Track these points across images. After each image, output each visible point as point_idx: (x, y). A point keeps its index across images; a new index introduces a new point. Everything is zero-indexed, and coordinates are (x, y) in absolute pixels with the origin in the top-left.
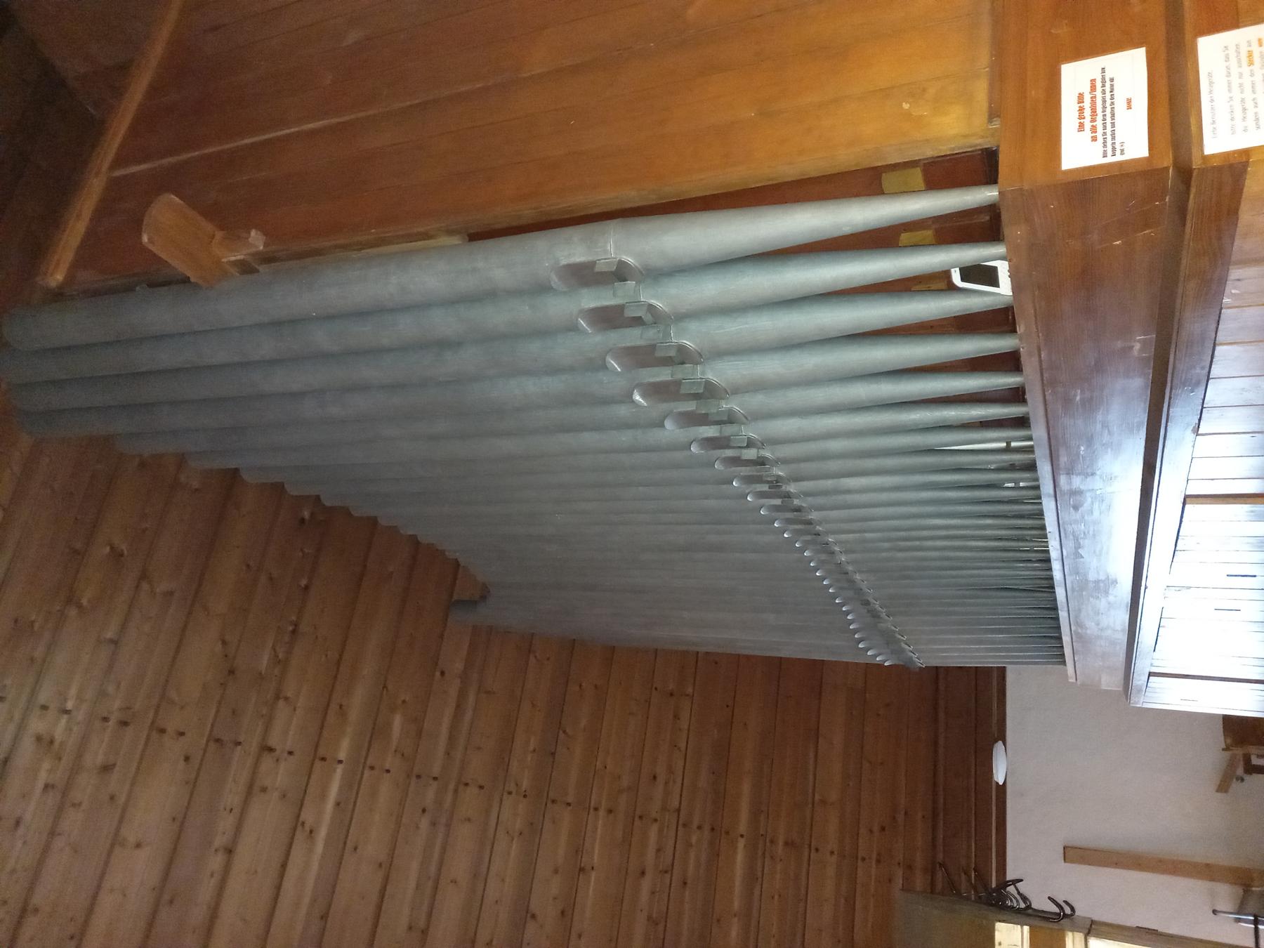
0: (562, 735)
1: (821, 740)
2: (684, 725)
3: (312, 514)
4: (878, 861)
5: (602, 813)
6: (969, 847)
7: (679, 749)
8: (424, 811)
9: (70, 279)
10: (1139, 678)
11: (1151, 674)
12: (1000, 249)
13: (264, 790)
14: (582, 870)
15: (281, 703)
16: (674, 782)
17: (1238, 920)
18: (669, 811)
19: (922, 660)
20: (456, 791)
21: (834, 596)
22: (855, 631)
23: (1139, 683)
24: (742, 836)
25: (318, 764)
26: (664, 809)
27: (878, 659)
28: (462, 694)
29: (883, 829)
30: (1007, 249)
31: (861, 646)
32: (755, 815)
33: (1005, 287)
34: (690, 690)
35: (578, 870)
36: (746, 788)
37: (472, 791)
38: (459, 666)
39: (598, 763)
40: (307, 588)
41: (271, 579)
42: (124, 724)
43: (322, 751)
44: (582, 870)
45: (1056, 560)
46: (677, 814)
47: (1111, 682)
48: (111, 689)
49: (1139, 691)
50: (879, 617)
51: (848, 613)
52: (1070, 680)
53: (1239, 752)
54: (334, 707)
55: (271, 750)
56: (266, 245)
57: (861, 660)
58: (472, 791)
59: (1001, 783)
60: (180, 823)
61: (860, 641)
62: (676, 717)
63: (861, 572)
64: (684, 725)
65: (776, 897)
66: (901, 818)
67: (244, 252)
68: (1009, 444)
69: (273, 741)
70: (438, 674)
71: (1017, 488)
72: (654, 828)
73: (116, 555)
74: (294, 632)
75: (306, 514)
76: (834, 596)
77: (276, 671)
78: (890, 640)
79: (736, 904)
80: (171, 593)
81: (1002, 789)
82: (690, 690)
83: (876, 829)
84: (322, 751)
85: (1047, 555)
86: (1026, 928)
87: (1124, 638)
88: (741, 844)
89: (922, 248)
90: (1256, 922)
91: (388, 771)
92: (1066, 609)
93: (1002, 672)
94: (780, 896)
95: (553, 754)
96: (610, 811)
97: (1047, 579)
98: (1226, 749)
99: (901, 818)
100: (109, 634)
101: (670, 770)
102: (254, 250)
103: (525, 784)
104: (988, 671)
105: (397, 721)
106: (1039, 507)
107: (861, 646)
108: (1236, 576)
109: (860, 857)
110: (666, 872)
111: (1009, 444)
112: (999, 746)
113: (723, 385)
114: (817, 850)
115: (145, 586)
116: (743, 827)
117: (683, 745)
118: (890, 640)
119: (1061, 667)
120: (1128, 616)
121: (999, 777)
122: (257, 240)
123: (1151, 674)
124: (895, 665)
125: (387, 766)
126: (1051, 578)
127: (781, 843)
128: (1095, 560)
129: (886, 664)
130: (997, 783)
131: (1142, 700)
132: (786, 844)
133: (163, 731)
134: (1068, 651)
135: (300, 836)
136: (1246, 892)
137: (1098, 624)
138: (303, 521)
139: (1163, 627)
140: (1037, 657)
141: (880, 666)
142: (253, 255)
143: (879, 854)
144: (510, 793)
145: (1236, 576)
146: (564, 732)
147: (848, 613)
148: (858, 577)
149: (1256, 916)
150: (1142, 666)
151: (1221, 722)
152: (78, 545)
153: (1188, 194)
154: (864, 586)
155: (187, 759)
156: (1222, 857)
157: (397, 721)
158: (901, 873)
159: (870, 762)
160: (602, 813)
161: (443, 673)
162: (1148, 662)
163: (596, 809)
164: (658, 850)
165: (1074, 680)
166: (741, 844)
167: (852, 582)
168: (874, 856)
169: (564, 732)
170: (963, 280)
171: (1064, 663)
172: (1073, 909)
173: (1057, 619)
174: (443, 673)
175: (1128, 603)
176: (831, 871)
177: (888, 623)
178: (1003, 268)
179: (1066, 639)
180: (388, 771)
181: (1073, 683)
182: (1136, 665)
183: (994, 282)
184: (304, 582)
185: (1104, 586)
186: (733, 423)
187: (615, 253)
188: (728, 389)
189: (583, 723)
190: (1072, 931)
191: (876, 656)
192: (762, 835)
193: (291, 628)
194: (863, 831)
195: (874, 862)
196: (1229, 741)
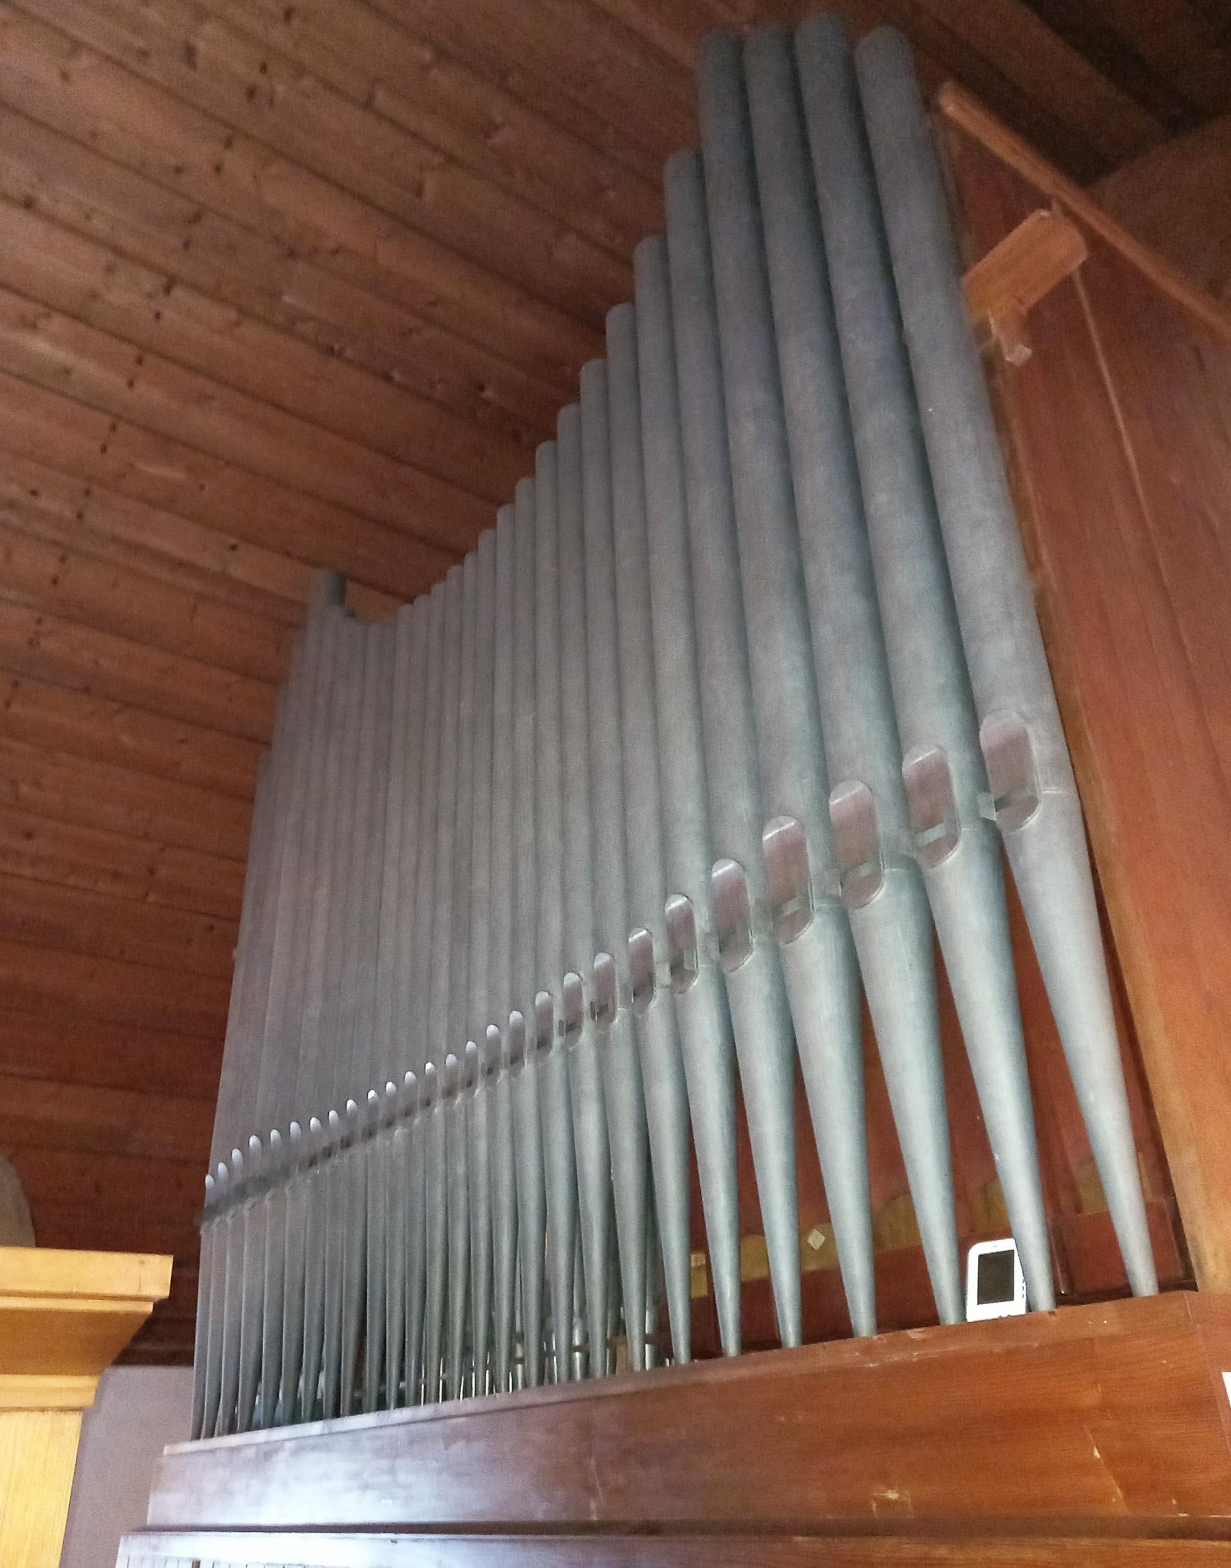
0: (115, 706)
2: (101, 886)
3: (487, 403)
8: (34, 493)
9: (949, 123)
12: (1044, 1301)
13: (110, 269)
15: (233, 316)
20: (55, 543)
21: (360, 1098)
25: (132, 352)
28: (199, 572)
30: (952, 1326)
31: (253, 1140)
33: (978, 1312)
37: (50, 566)
38: (238, 571)
40: (388, 378)
41: (411, 331)
42: (251, 93)
43: (150, 360)
45: (436, 1410)
48: (307, 83)
51: (323, 1119)
54: (209, 387)
55: (168, 290)
56: (1011, 365)
57: (216, 1141)
58: (50, 566)
60: (89, 143)
61: (264, 1139)
62: (116, 876)
63: (409, 1137)
64: (101, 886)
67: (1002, 337)
68: (578, 1349)
69: (178, 293)
70: (233, 541)
71: (572, 1349)
73: (490, 129)
74: (331, 350)
75: (489, 394)
76: (360, 1098)
77: (280, 319)
80: (419, 192)
82: (152, 898)
84: (150, 360)
85: (450, 1398)
89: (736, 1261)
91: (104, 450)
95: (87, 690)
97: (418, 1394)
100: (381, 97)
102: (1005, 349)
103: (48, 644)
105: (176, 474)
106: (433, 1399)
107: (253, 1140)
111: (521, 1361)
113: (801, 937)
115: (437, 160)
117: (71, 881)
119: (190, 1434)
122: (1018, 354)
125: (110, 450)
133: (228, 144)
135: (31, 309)
138: (482, 388)
141: (204, 1166)
142: (998, 346)
144: (39, 621)
146: (118, 711)
147: (323, 1119)
152: (514, 80)
153: (1212, 1539)
155: (179, 170)
157: (176, 474)
161: (234, 548)
169: (118, 711)
170: (983, 1258)
174: (234, 548)
178: (1015, 1307)
180: (104, 450)
183: (985, 1296)
184: (396, 375)
186: (720, 952)
187: (1046, 795)
188: (791, 944)
189: (127, 740)
191: (228, 1161)
193: (336, 347)
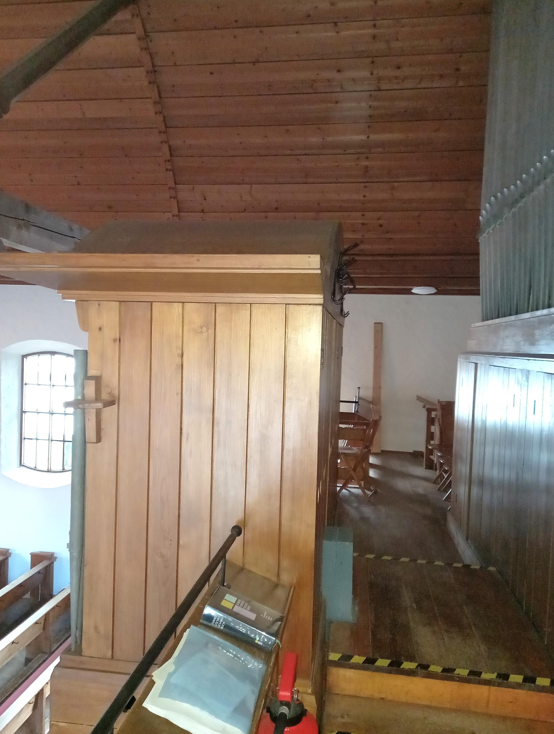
1: (430, 183)
4: (363, 224)
5: (372, 31)
6: (376, 274)
7: (419, 83)
10: (473, 359)
11: (476, 364)
14: (336, 24)
16: (398, 83)
17: (356, 396)
18: (379, 83)
19: (483, 239)
21: (527, 173)
22: (502, 193)
23: (471, 358)
24: (368, 137)
26: (379, 79)
27: (484, 211)
29: (381, 226)
31: (492, 198)
32: (382, 144)
34: (461, 84)
35: (336, 21)
36: (396, 136)
39: (405, 20)
44: (336, 24)
46: (377, 89)
47: (472, 344)
49: (466, 359)
50: (512, 207)
51: (515, 185)
52: (472, 325)
53: (438, 407)
59: (413, 291)
61: (496, 197)
62: (441, 76)
65: (336, 164)
66: (388, 236)
72: (365, 73)
76: (527, 173)
78: (496, 217)
79: (330, 139)
81: (408, 292)
83: (381, 222)
86: (319, 272)
87: (498, 351)
88: (364, 137)
90: (355, 402)
92: (516, 319)
93: (476, 293)
94: (337, 166)
96: (374, 37)
97: (537, 306)
98: (439, 402)
99: (388, 236)
101: (405, 78)
104: (478, 284)
108: (535, 405)
109: (364, 213)
110: (342, 88)
112: (433, 290)
114: (365, 187)
116: (373, 137)
117: (423, 85)
118: (496, 217)
119: (481, 318)
120: (511, 352)
121: (415, 290)
123: (476, 364)
124: (480, 223)
126: (537, 309)
127: (367, 163)
128: (548, 333)
129: (481, 218)
130: (412, 289)
131: (461, 360)
132: (367, 167)
134: (490, 322)
136: (370, 402)
137: (506, 337)
139: (504, 370)
140: (486, 303)
143: (367, 224)
145: (535, 405)
147: (515, 185)
148: (542, 187)
149: (358, 402)
150: (481, 360)
151: (452, 401)
154: (535, 193)
156: (384, 395)
158: (358, 237)
159: (419, 216)
160: (372, 31)
162: (483, 362)
163: (374, 26)
164: (354, 80)
165: (472, 327)
166: (364, 137)
167: (538, 184)
168: (365, 221)
171: (483, 320)
172: (346, 316)
173: (510, 315)
175: (519, 352)
176: (355, 197)
177: (508, 214)
179: (497, 321)
181: (471, 326)
182: (482, 357)
185: (533, 343)
190: (324, 298)
192: (370, 151)
194: (379, 214)
195: (362, 221)
196: (444, 403)
